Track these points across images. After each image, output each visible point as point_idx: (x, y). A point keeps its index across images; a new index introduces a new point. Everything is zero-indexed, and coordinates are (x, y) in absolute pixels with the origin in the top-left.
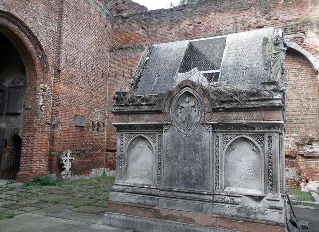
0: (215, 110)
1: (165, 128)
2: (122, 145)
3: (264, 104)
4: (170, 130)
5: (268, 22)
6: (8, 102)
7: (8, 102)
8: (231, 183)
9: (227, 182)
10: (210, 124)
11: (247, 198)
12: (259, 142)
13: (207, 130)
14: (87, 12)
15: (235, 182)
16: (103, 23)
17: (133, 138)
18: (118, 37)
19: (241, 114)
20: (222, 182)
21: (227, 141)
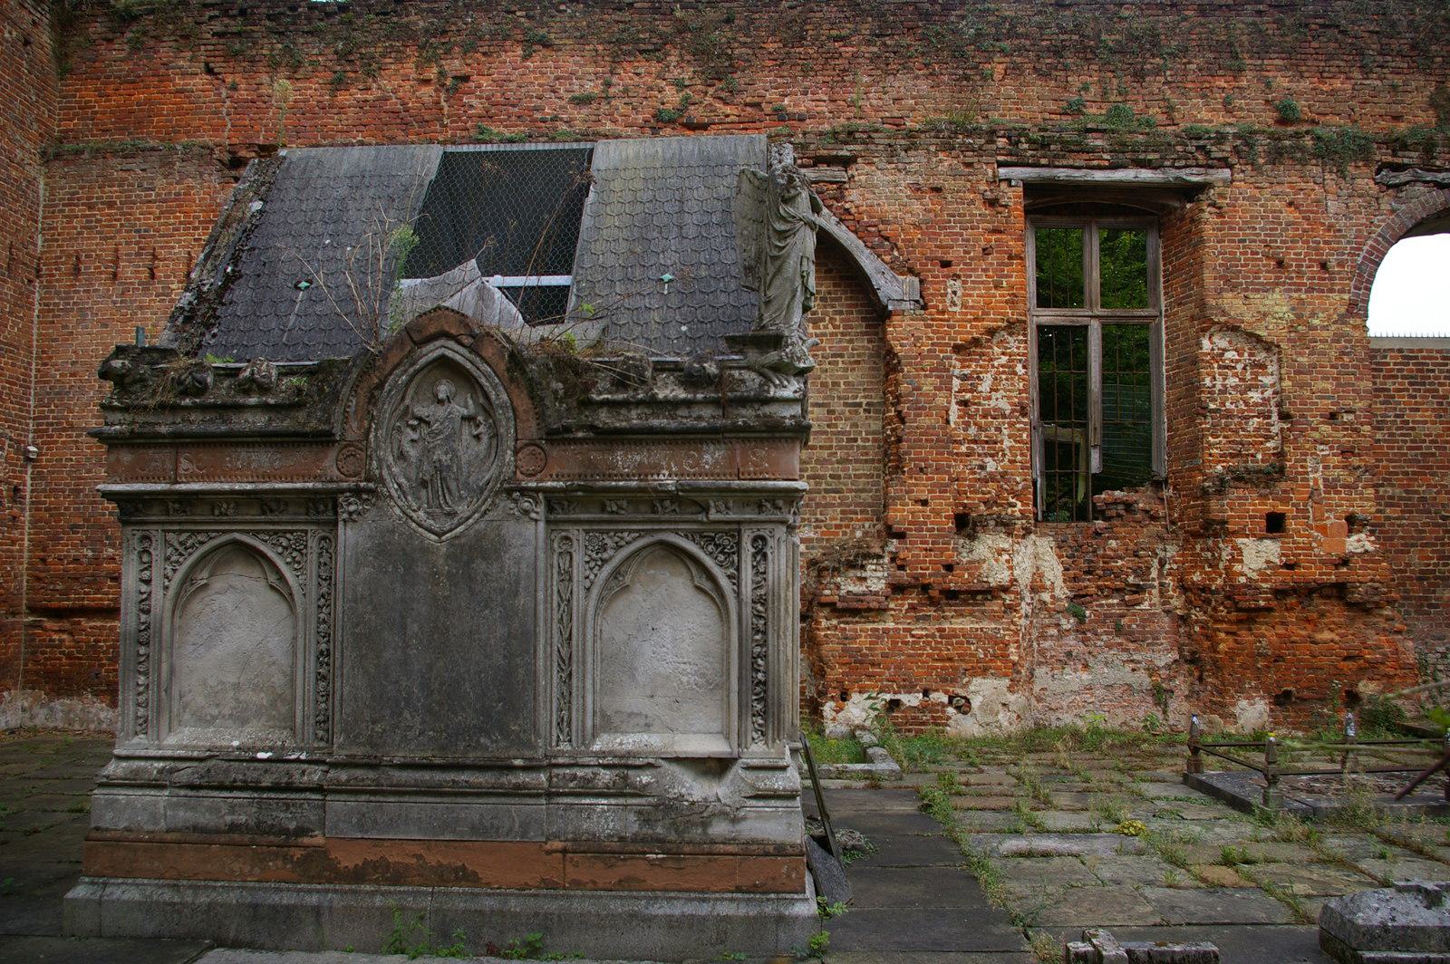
8: (616, 720)
11: (675, 769)
13: (526, 512)
21: (605, 556)
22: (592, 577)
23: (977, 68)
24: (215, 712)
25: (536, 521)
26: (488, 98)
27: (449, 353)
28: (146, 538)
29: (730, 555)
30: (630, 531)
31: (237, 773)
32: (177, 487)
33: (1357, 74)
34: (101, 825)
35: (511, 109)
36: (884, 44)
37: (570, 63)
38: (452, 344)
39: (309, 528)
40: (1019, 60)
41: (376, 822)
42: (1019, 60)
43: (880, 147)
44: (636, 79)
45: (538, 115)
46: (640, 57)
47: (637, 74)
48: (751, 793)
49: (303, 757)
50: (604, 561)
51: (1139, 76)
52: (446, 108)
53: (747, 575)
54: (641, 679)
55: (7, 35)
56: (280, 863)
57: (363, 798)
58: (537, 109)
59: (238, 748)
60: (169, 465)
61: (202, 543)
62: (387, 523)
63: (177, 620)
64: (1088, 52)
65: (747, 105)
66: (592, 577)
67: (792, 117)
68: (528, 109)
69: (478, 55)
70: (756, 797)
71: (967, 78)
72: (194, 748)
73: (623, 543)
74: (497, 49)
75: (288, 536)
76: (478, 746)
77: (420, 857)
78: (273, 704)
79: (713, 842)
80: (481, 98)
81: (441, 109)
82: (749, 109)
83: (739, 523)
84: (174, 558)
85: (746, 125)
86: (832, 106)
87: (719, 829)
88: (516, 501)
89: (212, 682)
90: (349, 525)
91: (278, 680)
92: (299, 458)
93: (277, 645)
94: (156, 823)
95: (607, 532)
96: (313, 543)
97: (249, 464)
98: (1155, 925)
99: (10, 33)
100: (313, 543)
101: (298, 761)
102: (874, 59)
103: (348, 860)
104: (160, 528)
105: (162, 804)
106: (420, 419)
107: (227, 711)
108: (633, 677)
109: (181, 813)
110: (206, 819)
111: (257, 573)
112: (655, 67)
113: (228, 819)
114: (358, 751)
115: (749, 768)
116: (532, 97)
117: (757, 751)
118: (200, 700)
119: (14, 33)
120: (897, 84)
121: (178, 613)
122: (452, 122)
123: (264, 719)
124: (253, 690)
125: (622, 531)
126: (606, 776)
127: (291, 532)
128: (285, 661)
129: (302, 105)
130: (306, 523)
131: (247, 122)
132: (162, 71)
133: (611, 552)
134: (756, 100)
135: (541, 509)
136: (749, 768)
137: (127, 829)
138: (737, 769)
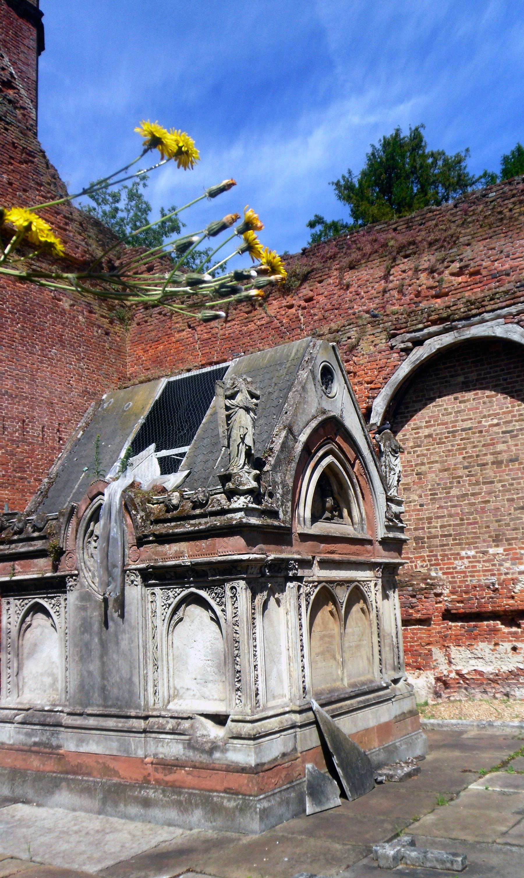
0: (141, 542)
1: (70, 583)
2: (10, 623)
3: (217, 521)
4: (77, 587)
5: (460, 279)
6: (173, 677)
7: (173, 677)
8: (181, 692)
9: (175, 688)
10: (136, 570)
11: (202, 719)
12: (218, 599)
13: (132, 582)
14: (52, 310)
15: (188, 689)
16: (99, 327)
17: (27, 606)
18: (141, 353)
19: (183, 546)
20: (163, 691)
21: (169, 602)
22: (165, 614)
25: (137, 585)
29: (220, 597)
32: (14, 578)
43: (433, 314)
52: (302, 319)
53: (229, 608)
55: (95, 334)
61: (26, 604)
63: (20, 642)
66: (165, 614)
73: (176, 595)
85: (472, 287)
91: (223, 650)
95: (169, 589)
99: (97, 332)
115: (233, 721)
119: (99, 331)
121: (21, 638)
126: (170, 724)
129: (232, 335)
131: (208, 351)
132: (169, 332)
133: (172, 600)
135: (139, 579)
136: (233, 721)
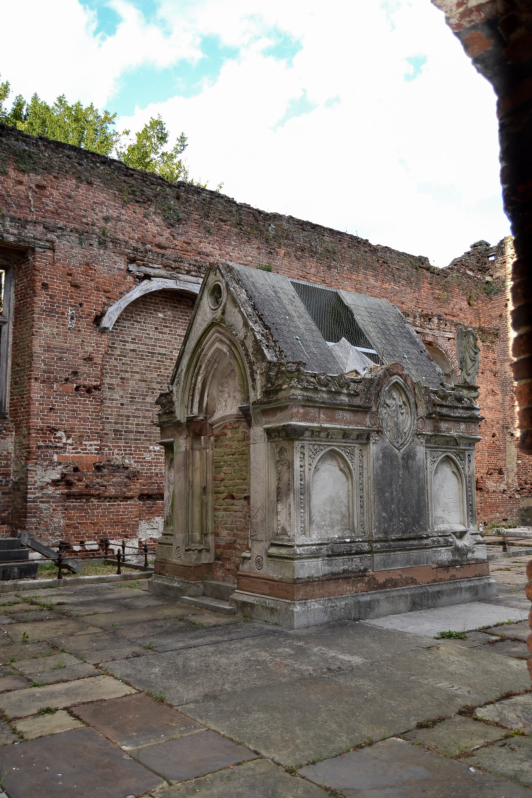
23: (274, 249)
24: (323, 524)
26: (57, 203)
27: (398, 381)
28: (303, 447)
30: (441, 451)
31: (343, 548)
33: (392, 284)
34: (300, 577)
35: (70, 213)
36: (241, 229)
37: (102, 197)
38: (399, 377)
39: (357, 445)
40: (290, 250)
41: (388, 563)
42: (290, 250)
44: (134, 215)
45: (84, 220)
46: (136, 204)
47: (135, 212)
48: (475, 542)
49: (360, 540)
50: (434, 462)
51: (329, 268)
54: (441, 504)
56: (361, 584)
57: (384, 554)
58: (84, 216)
59: (338, 538)
60: (317, 415)
62: (385, 445)
64: (313, 253)
65: (184, 242)
67: (204, 253)
68: (78, 215)
69: (51, 177)
70: (477, 544)
71: (271, 253)
72: (324, 540)
74: (62, 176)
75: (349, 448)
76: (413, 531)
77: (401, 576)
78: (342, 520)
79: (468, 560)
80: (53, 201)
81: (30, 201)
82: (185, 244)
83: (465, 450)
84: (313, 456)
86: (220, 252)
87: (470, 555)
88: (419, 439)
89: (322, 511)
90: (375, 445)
91: (344, 509)
92: (359, 417)
93: (343, 495)
94: (318, 573)
96: (357, 451)
97: (343, 417)
98: (126, 696)
100: (357, 451)
101: (359, 541)
102: (237, 234)
103: (381, 580)
104: (308, 442)
105: (320, 564)
106: (387, 405)
107: (327, 523)
108: (439, 504)
109: (327, 568)
110: (335, 569)
111: (334, 463)
112: (143, 211)
113: (342, 568)
114: (381, 536)
115: (472, 534)
116: (81, 209)
117: (473, 529)
118: (318, 519)
120: (245, 249)
122: (36, 211)
123: (340, 525)
124: (336, 513)
125: (438, 451)
127: (350, 447)
128: (346, 501)
130: (356, 443)
134: (190, 241)
136: (472, 534)
137: (308, 577)
138: (468, 535)
